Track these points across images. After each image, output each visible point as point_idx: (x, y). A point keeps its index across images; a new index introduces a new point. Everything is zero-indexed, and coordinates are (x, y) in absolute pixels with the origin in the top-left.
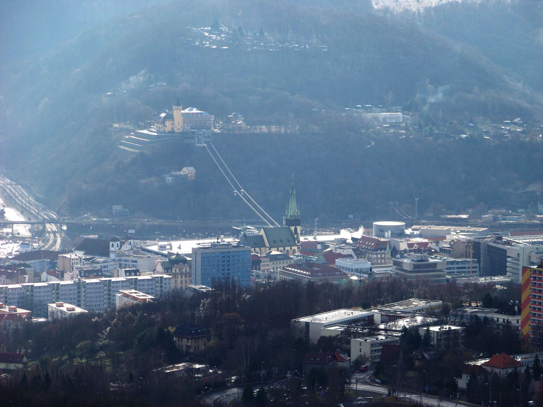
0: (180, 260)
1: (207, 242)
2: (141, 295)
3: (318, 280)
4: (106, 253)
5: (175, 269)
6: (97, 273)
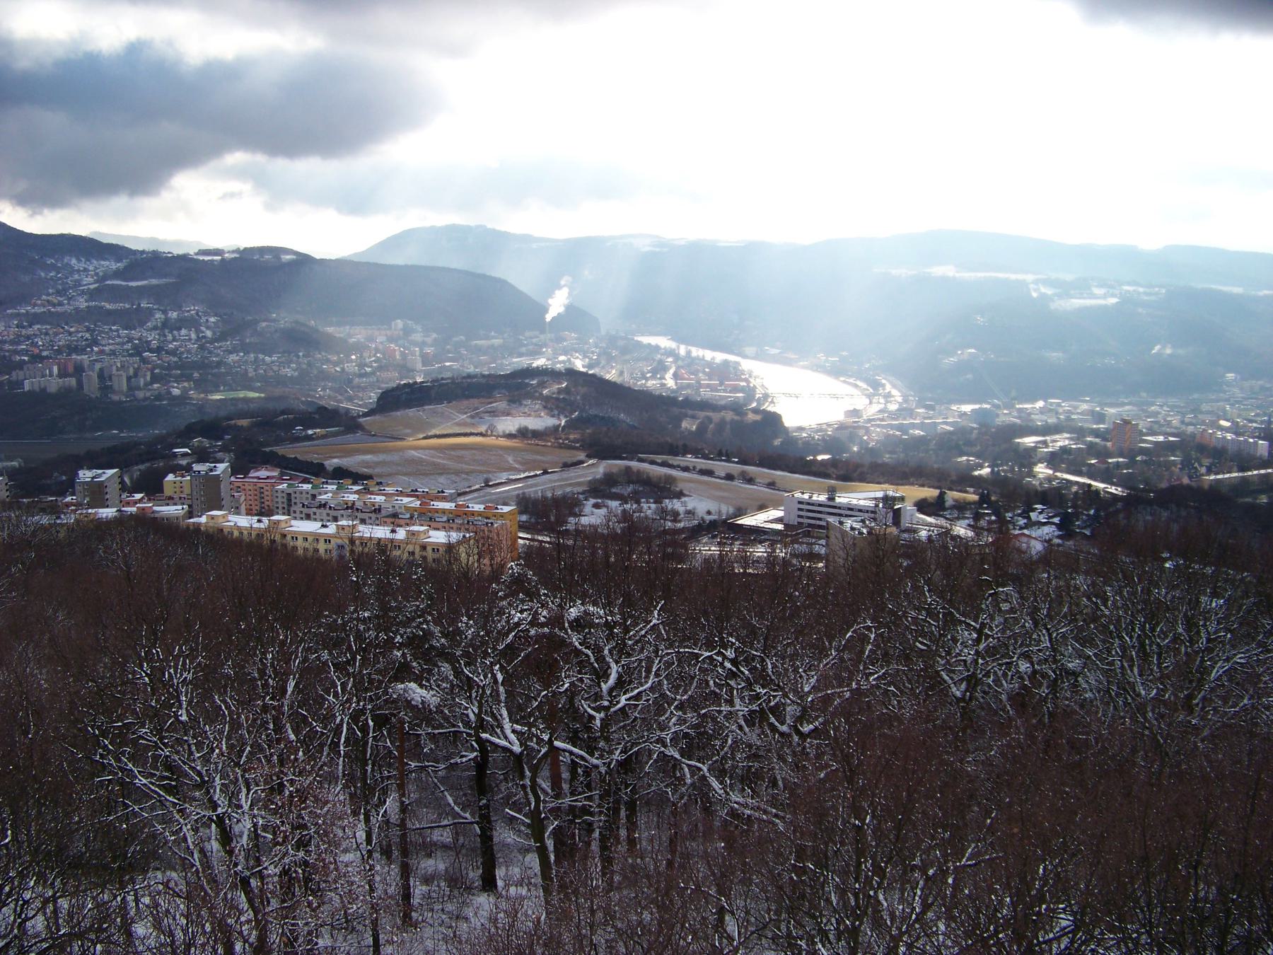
0: (965, 414)
1: (977, 406)
2: (948, 428)
3: (1024, 424)
4: (934, 410)
5: (964, 418)
6: (930, 418)
